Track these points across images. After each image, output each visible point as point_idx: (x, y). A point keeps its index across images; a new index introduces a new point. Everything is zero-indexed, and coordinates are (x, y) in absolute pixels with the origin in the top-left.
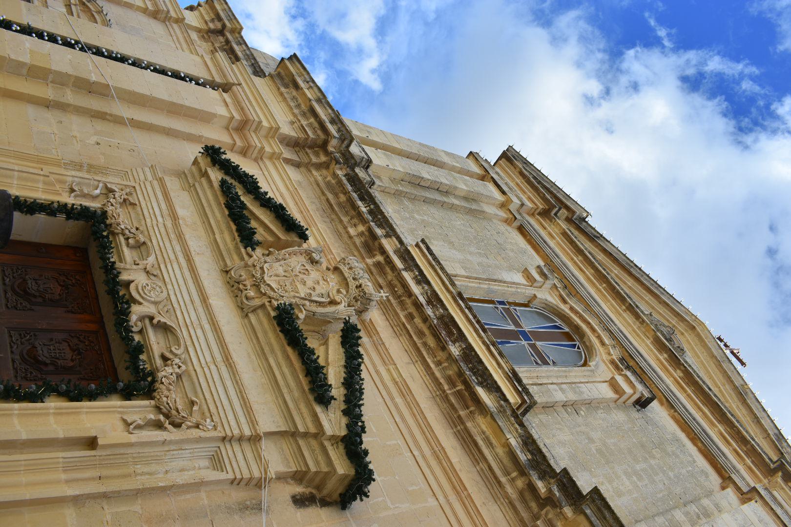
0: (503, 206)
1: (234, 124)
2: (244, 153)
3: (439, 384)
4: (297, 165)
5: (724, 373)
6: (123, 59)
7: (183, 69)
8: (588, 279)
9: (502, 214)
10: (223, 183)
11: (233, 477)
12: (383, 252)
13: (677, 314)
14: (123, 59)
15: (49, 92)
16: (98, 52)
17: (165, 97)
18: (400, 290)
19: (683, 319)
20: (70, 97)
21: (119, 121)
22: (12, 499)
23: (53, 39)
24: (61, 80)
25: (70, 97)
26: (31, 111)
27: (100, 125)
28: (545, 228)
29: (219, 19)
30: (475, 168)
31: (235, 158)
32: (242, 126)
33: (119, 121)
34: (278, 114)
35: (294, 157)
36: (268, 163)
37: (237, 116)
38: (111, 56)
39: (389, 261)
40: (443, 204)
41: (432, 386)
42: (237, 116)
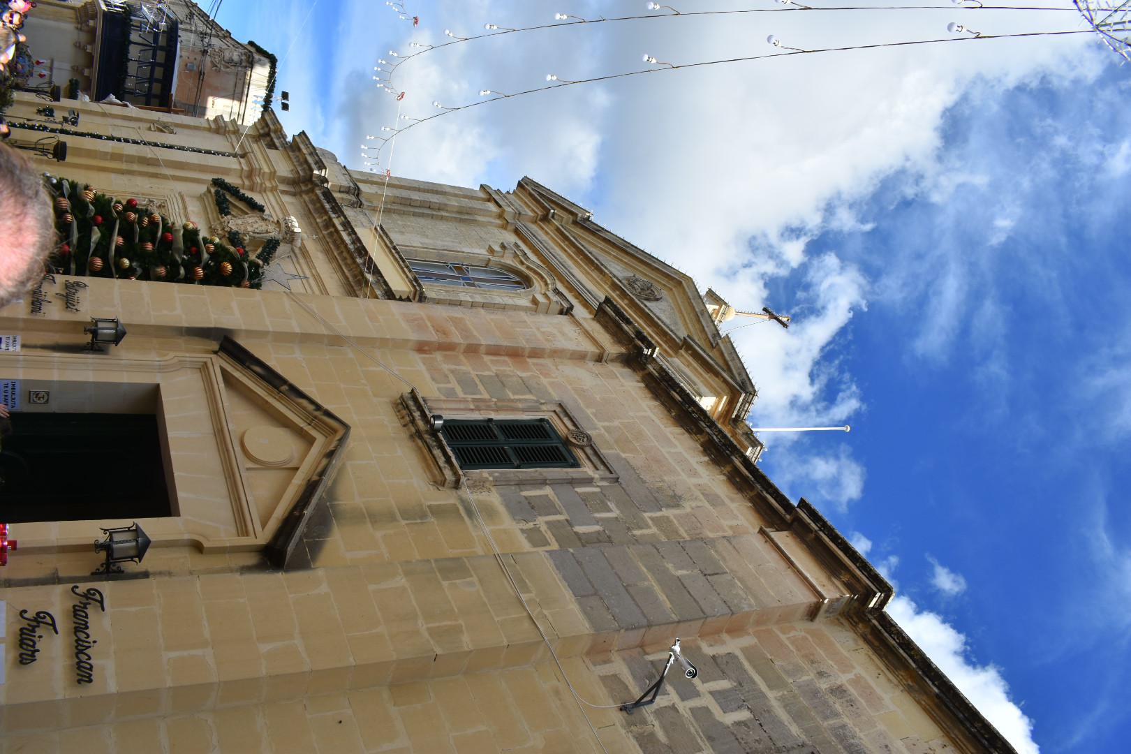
0: (501, 216)
1: (245, 174)
2: (251, 189)
3: (347, 278)
4: (294, 195)
5: (605, 240)
6: (171, 147)
7: (213, 149)
8: (570, 255)
9: (498, 222)
10: (217, 193)
11: (813, 599)
12: (334, 226)
13: (667, 276)
14: (171, 147)
15: (124, 166)
16: (156, 145)
17: (196, 162)
18: (339, 242)
19: (672, 279)
20: (136, 167)
21: (165, 177)
22: (212, 326)
23: (126, 141)
24: (131, 159)
25: (136, 167)
26: (113, 176)
27: (154, 180)
28: (598, 268)
29: (267, 125)
30: (482, 195)
31: (248, 194)
32: (250, 175)
33: (165, 177)
34: (283, 166)
35: (292, 190)
36: (270, 194)
37: (245, 168)
38: (163, 146)
39: (337, 231)
40: (432, 217)
41: (342, 278)
42: (245, 168)
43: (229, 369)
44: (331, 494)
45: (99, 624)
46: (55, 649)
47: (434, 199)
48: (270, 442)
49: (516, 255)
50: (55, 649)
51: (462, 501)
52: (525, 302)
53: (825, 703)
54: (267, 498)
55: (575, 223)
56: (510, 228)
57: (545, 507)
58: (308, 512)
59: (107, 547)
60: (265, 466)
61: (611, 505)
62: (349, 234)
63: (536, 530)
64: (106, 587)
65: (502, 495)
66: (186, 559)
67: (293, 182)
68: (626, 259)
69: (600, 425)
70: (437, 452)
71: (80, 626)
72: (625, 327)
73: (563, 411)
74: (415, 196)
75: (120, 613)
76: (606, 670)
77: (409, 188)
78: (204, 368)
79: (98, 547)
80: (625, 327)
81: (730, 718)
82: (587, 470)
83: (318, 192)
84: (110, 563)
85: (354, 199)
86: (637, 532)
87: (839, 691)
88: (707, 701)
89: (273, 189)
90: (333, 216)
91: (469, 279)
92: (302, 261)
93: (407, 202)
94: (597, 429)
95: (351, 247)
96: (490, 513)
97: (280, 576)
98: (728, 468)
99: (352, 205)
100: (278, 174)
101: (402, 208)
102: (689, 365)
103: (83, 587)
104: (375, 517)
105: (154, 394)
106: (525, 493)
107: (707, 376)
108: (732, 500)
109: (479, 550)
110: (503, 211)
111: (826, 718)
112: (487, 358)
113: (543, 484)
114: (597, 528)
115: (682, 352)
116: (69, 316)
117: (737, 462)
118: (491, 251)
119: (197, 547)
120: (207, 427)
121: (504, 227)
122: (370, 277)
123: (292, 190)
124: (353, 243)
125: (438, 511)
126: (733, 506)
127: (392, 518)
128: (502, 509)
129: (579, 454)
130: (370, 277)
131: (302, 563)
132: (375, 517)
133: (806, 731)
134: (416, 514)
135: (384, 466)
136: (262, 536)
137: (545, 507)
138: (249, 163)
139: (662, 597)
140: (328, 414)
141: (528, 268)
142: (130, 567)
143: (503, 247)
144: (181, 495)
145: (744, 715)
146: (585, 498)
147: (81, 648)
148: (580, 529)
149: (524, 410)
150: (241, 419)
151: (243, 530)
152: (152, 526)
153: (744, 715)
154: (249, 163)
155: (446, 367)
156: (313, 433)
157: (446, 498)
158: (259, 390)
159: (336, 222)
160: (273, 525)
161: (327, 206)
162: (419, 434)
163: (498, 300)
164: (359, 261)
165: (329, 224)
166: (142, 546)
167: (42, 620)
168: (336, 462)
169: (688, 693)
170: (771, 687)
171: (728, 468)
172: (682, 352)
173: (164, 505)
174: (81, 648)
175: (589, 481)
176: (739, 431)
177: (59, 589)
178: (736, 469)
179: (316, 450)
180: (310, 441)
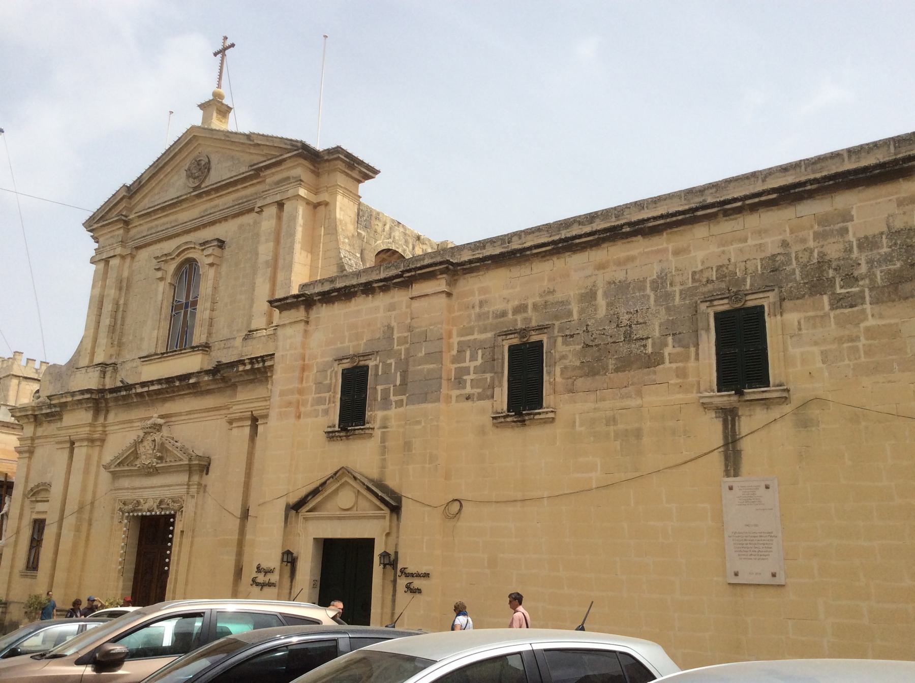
4: (107, 412)
36: (107, 429)
43: (308, 509)
44: (371, 481)
45: (411, 569)
46: (417, 583)
47: (108, 307)
48: (345, 498)
49: (166, 261)
50: (417, 583)
51: (379, 428)
52: (212, 272)
53: (484, 314)
54: (367, 504)
55: (130, 198)
56: (134, 253)
57: (386, 393)
58: (380, 494)
59: (385, 565)
60: (356, 503)
61: (389, 362)
62: (153, 385)
63: (396, 402)
64: (400, 566)
65: (379, 409)
66: (392, 539)
67: (97, 411)
68: (168, 169)
69: (346, 344)
70: (357, 432)
71: (412, 575)
72: (289, 301)
73: (339, 360)
74: (106, 321)
75: (406, 561)
76: (454, 399)
77: (98, 323)
78: (306, 519)
79: (384, 568)
80: (289, 301)
81: (480, 361)
82: (371, 364)
83: (109, 396)
84: (390, 561)
85: (110, 369)
86: (403, 357)
87: (481, 304)
88: (473, 364)
89: (104, 426)
90: (134, 391)
91: (187, 304)
92: (173, 419)
93: (112, 329)
94: (350, 346)
95: (164, 386)
96: (385, 419)
97: (403, 509)
98: (377, 290)
99: (115, 370)
100: (90, 421)
101: (118, 332)
102: (273, 174)
103: (399, 573)
104: (383, 467)
105: (316, 540)
106: (379, 399)
107: (283, 167)
108: (393, 297)
109: (401, 430)
110: (120, 255)
111: (488, 318)
112: (304, 385)
113: (376, 389)
114: (398, 374)
115: (262, 174)
116: (277, 572)
117: (375, 285)
118: (162, 279)
119: (388, 535)
120: (336, 522)
121: (133, 257)
122: (192, 381)
123: (104, 412)
124: (161, 384)
125: (383, 440)
126: (396, 299)
127: (384, 460)
128: (385, 413)
129: (362, 363)
130: (192, 381)
131: (399, 499)
132: (383, 467)
133: (491, 330)
134: (384, 450)
135: (361, 455)
136: (387, 511)
137: (386, 393)
138: (82, 440)
139: (432, 366)
140: (336, 473)
141: (178, 255)
142: (392, 557)
143: (158, 269)
144: (366, 536)
145: (480, 352)
146: (384, 372)
147: (418, 575)
148: (398, 383)
149: (336, 380)
150: (331, 508)
151: (384, 517)
152: (378, 550)
153: (480, 352)
154: (82, 440)
155: (309, 408)
156: (343, 481)
157: (378, 433)
158: (319, 498)
159: (139, 390)
160: (382, 506)
161: (124, 393)
162: (347, 436)
163: (209, 291)
164: (177, 384)
165: (141, 395)
166: (385, 555)
167: (408, 587)
168: (359, 477)
169: (466, 371)
170: (473, 334)
171: (377, 290)
172: (262, 174)
173: (369, 544)
174: (418, 575)
175: (377, 366)
176: (326, 158)
177: (398, 580)
178: (379, 287)
179: (352, 482)
180: (346, 483)
